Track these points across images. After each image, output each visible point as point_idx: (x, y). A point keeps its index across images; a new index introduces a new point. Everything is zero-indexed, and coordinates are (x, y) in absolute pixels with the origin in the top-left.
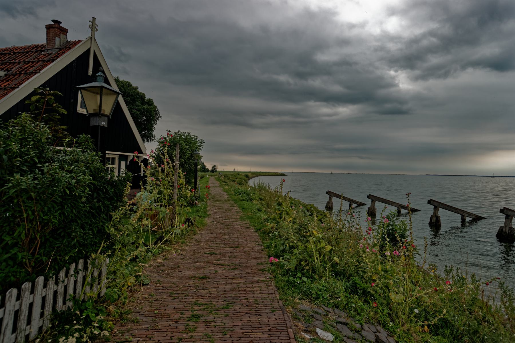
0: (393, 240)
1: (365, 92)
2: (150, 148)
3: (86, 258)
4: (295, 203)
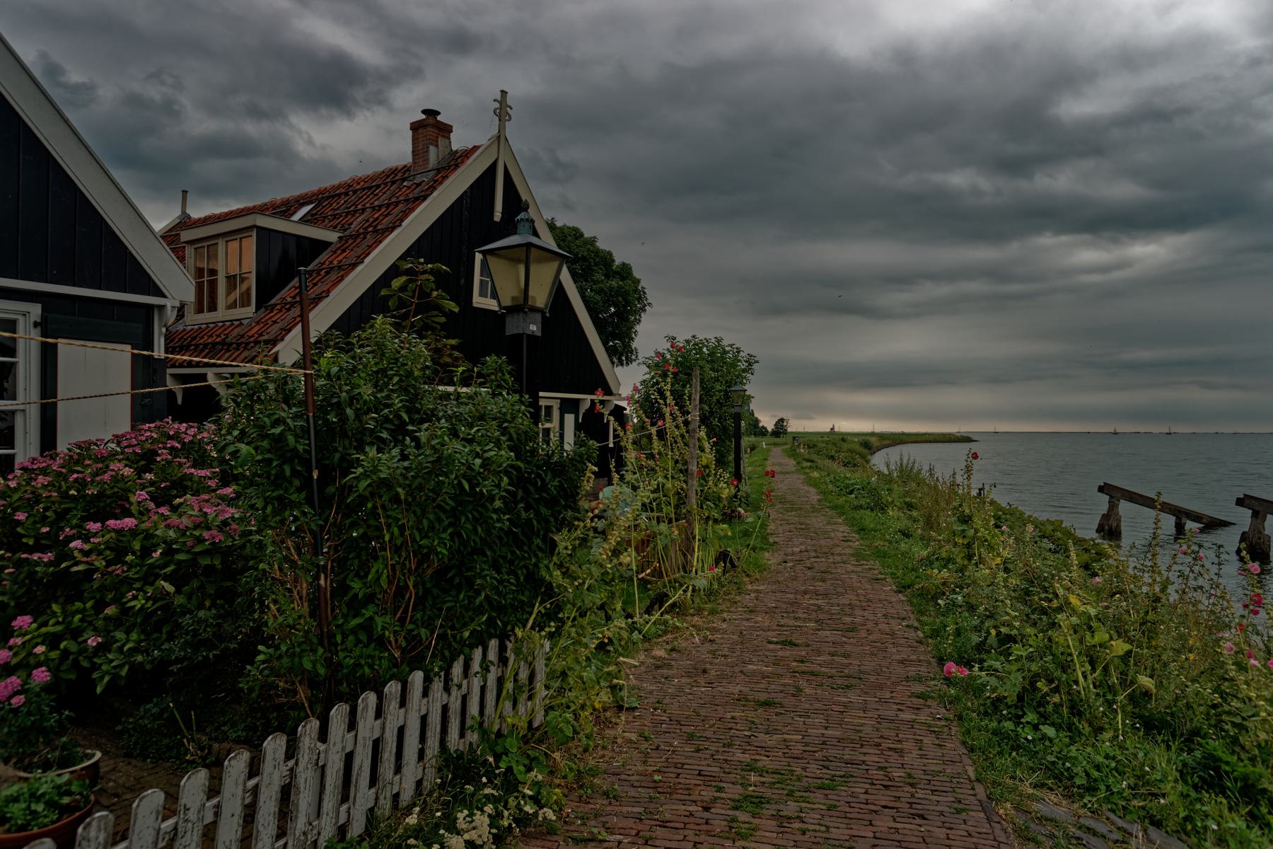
2: (628, 381)
3: (503, 637)
4: (1004, 517)
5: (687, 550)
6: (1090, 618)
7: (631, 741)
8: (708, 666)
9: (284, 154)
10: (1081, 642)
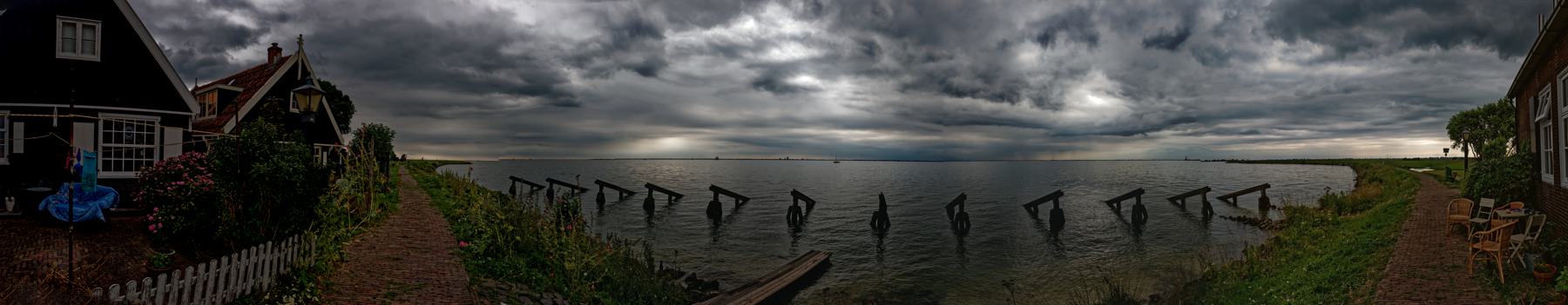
0: (567, 217)
1: (542, 86)
2: (347, 139)
3: (300, 233)
4: (482, 190)
9: (224, 62)
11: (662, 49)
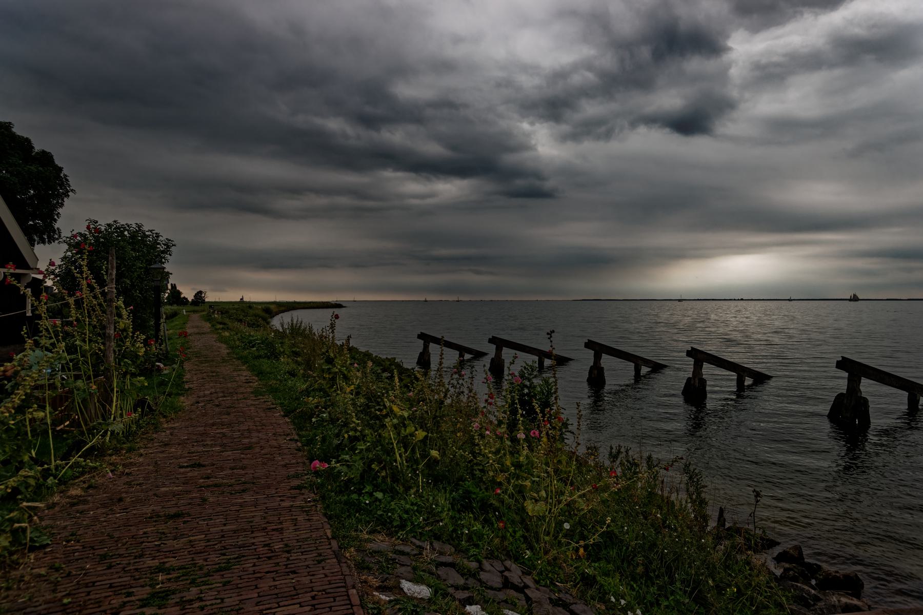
0: (531, 412)
1: (477, 157)
5: (106, 399)
6: (404, 419)
7: (40, 576)
8: (124, 495)
10: (399, 434)
11: (722, 75)
